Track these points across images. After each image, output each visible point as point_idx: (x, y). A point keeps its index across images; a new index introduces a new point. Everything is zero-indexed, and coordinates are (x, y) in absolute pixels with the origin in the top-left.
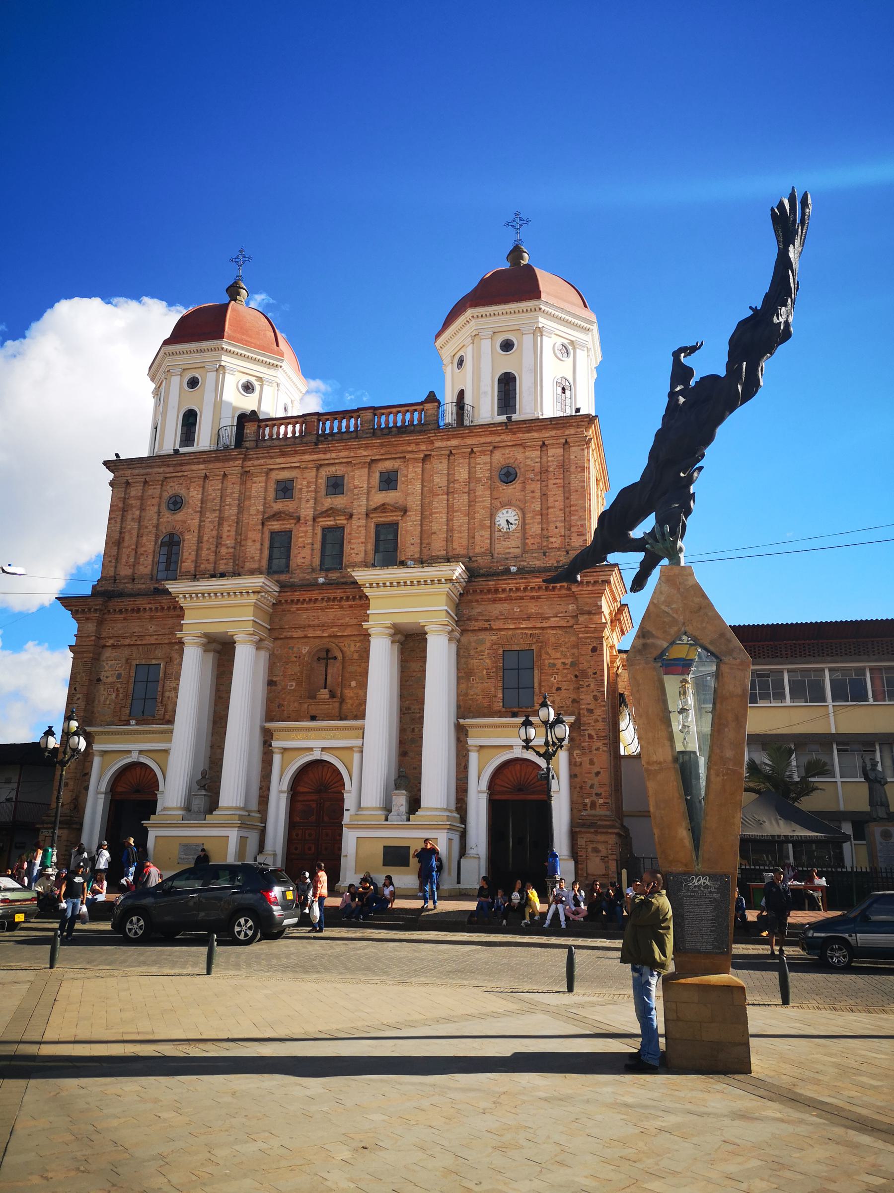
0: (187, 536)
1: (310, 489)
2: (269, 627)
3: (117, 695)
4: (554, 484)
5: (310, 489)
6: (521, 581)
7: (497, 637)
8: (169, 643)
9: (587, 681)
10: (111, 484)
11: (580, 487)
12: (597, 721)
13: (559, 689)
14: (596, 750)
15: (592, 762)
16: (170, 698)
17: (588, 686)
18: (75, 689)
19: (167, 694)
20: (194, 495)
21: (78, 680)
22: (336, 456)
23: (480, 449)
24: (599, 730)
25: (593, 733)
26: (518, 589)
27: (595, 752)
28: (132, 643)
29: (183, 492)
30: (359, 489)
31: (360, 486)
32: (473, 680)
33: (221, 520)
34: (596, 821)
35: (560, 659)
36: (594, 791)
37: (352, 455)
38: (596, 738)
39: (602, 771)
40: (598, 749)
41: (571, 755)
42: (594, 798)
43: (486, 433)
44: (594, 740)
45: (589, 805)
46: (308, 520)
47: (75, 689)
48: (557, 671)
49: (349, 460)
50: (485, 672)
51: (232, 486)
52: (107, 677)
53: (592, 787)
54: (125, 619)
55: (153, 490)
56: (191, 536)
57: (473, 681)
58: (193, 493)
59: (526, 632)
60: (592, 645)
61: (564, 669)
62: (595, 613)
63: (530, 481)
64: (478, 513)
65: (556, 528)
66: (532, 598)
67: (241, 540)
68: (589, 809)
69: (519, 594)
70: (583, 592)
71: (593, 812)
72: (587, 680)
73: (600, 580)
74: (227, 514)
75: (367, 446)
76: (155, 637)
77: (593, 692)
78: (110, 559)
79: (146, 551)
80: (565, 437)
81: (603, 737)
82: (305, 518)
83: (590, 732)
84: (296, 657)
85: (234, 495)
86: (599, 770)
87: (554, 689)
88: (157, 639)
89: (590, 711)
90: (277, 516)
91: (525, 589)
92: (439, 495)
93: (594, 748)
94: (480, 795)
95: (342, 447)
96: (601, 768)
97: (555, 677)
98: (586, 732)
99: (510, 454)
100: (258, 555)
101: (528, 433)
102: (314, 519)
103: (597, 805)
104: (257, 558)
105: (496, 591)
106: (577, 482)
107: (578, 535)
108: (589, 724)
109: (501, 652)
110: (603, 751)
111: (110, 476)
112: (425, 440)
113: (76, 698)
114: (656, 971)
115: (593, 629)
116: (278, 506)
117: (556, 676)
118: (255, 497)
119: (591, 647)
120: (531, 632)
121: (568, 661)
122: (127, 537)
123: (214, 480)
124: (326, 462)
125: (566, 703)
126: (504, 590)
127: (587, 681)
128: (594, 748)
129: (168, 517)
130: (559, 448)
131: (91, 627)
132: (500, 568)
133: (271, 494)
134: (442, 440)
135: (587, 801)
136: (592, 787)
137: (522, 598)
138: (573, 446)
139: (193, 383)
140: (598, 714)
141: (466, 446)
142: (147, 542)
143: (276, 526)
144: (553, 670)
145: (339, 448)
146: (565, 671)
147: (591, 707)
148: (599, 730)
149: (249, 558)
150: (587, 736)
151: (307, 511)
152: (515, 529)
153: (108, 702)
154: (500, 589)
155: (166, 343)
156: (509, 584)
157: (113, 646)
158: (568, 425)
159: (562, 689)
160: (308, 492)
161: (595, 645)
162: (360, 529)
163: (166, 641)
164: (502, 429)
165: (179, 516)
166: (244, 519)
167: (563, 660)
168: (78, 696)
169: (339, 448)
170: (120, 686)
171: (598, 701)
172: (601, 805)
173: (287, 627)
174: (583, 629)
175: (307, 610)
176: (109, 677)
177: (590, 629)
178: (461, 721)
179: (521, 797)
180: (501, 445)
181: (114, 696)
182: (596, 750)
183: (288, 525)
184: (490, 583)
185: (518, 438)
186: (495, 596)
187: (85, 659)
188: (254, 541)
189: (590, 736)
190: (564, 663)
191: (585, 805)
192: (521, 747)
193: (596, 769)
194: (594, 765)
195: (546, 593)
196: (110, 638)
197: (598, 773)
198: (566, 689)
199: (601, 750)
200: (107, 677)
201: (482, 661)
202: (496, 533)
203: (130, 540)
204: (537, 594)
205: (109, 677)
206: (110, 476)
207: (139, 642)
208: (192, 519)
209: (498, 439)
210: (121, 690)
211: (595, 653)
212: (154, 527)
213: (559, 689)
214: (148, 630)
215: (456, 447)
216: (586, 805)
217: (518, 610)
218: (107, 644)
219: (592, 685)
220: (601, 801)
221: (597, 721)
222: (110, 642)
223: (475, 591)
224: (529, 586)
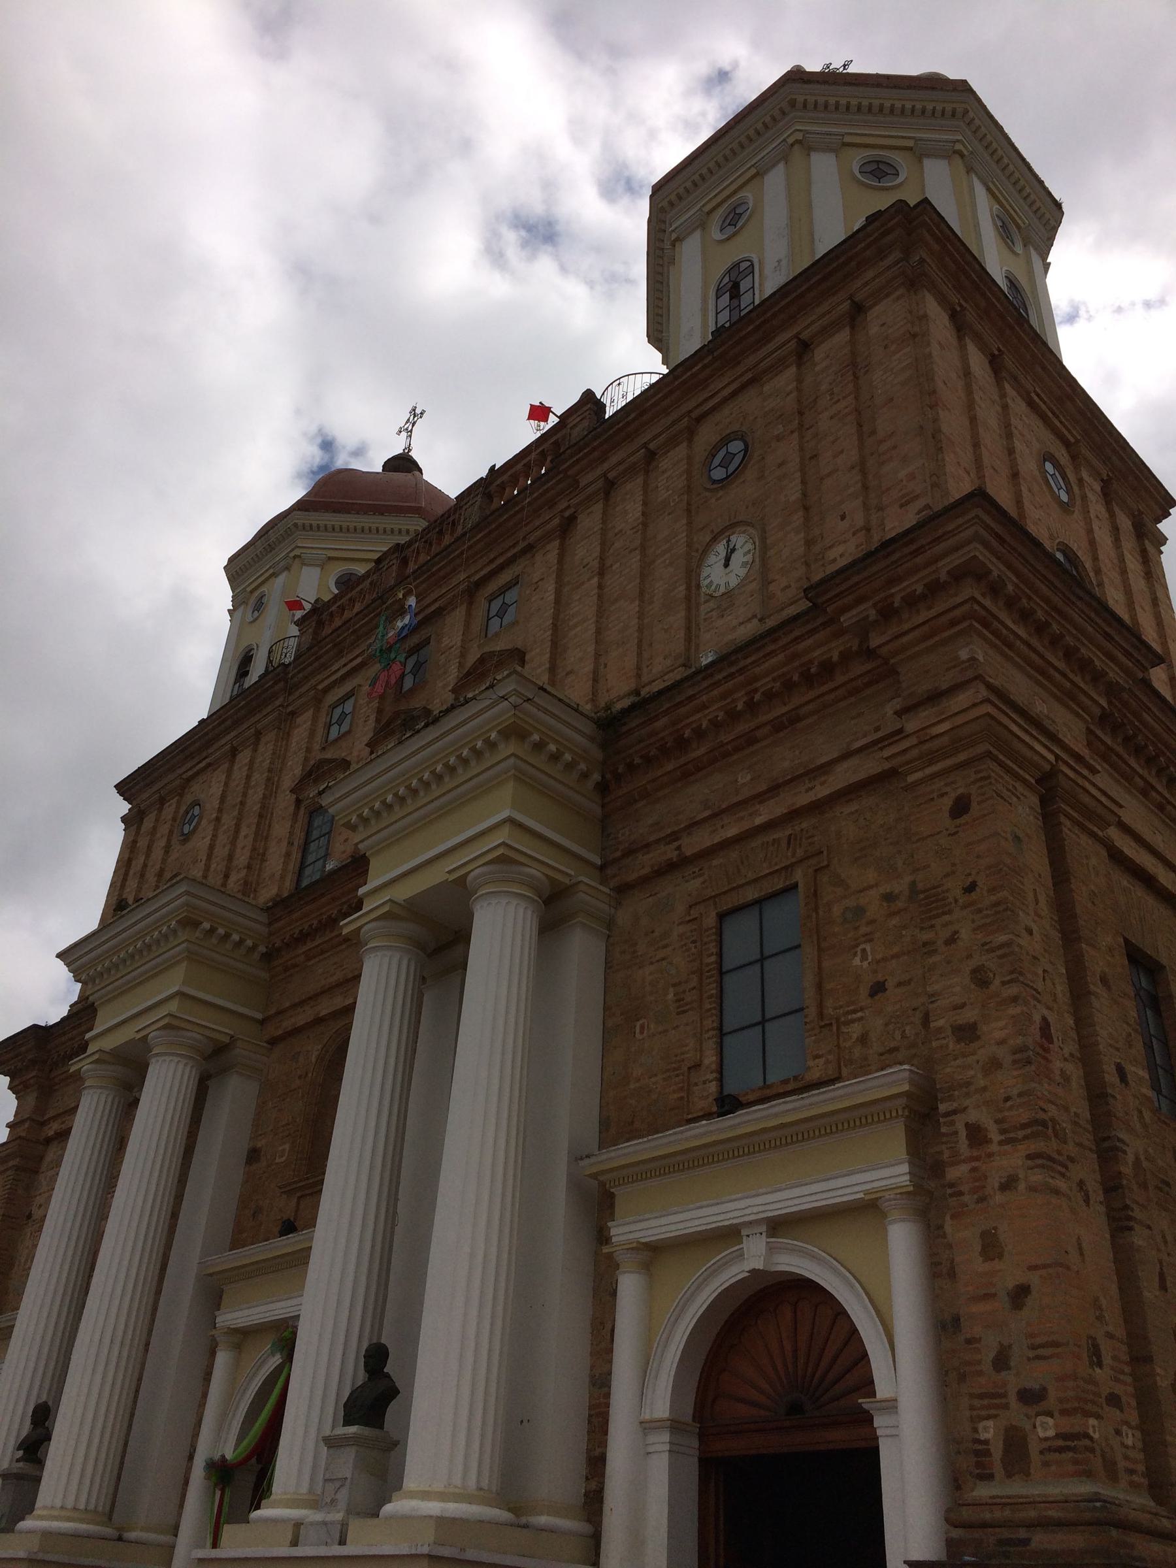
2: (259, 1016)
4: (831, 418)
6: (730, 684)
7: (701, 879)
9: (945, 925)
10: (124, 819)
12: (994, 1065)
13: (878, 989)
15: (991, 1247)
17: (952, 940)
24: (1007, 1099)
26: (733, 716)
27: (999, 1198)
32: (642, 1027)
34: (1022, 1534)
35: (876, 885)
36: (1013, 1382)
39: (1034, 1279)
40: (1008, 1185)
42: (1016, 1413)
44: (994, 1147)
45: (997, 1451)
48: (868, 929)
50: (671, 996)
53: (1001, 1361)
57: (642, 1033)
59: (776, 836)
60: (953, 795)
61: (891, 915)
66: (778, 726)
68: (998, 1469)
69: (742, 727)
70: (905, 639)
71: (1016, 1488)
72: (947, 918)
73: (943, 576)
77: (970, 956)
81: (1024, 1126)
83: (973, 1116)
87: (864, 991)
89: (967, 1033)
91: (752, 706)
92: (583, 583)
93: (994, 1182)
96: (1033, 1268)
97: (864, 950)
103: (1034, 1448)
105: (682, 744)
107: (902, 506)
108: (968, 1084)
109: (711, 920)
110: (1032, 1189)
111: (124, 807)
115: (945, 740)
117: (868, 947)
119: (948, 802)
120: (788, 832)
121: (900, 886)
125: (904, 1036)
126: (700, 734)
127: (945, 925)
128: (994, 1182)
131: (31, 1099)
135: (989, 1431)
136: (1001, 1361)
137: (750, 740)
140: (998, 1035)
144: (856, 928)
146: (895, 921)
147: (969, 1015)
148: (1007, 1099)
150: (963, 1133)
156: (704, 707)
158: (853, 264)
159: (890, 984)
161: (960, 791)
164: (705, 367)
167: (885, 888)
171: (993, 987)
174: (915, 753)
175: (323, 952)
177: (936, 743)
184: (659, 724)
186: (682, 760)
189: (976, 1135)
190: (889, 898)
191: (981, 1452)
192: (764, 1228)
193: (1010, 1274)
194: (1001, 1256)
195: (812, 694)
197: (1020, 1294)
198: (899, 984)
199: (1022, 1186)
201: (664, 963)
204: (785, 709)
206: (124, 807)
211: (965, 818)
213: (878, 989)
216: (988, 1453)
217: (749, 777)
219: (965, 934)
220: (1046, 1428)
221: (994, 1065)
223: (631, 768)
224: (756, 691)
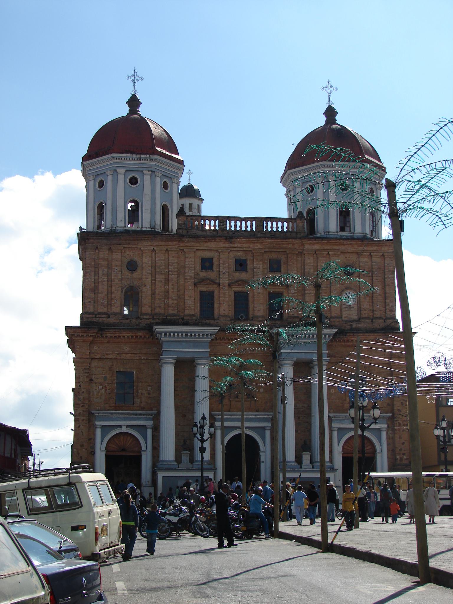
0: (144, 289)
1: (225, 266)
3: (106, 390)
5: (225, 266)
8: (140, 359)
11: (390, 283)
14: (403, 431)
16: (143, 394)
18: (80, 386)
19: (140, 391)
20: (146, 261)
21: (81, 380)
22: (241, 246)
23: (333, 253)
25: (401, 422)
28: (114, 357)
29: (137, 259)
30: (257, 269)
31: (258, 267)
33: (167, 281)
37: (251, 246)
38: (402, 425)
41: (387, 433)
42: (401, 456)
43: (337, 243)
46: (225, 286)
47: (80, 386)
49: (250, 249)
51: (172, 258)
52: (97, 378)
54: (108, 342)
55: (116, 256)
56: (147, 290)
58: (145, 260)
62: (402, 357)
63: (362, 276)
64: (333, 292)
65: (378, 306)
67: (180, 295)
74: (170, 277)
75: (262, 242)
76: (129, 355)
78: (89, 300)
79: (115, 297)
80: (383, 252)
82: (223, 284)
83: (399, 422)
84: (224, 372)
85: (174, 265)
86: (403, 441)
88: (131, 356)
90: (202, 281)
94: (102, 452)
95: (245, 241)
98: (397, 422)
99: (349, 257)
100: (193, 306)
101: (361, 247)
102: (229, 285)
104: (193, 308)
106: (389, 280)
112: (299, 243)
113: (81, 392)
114: (142, 512)
116: (203, 274)
118: (188, 267)
122: (100, 287)
123: (159, 253)
124: (235, 249)
129: (128, 275)
130: (378, 257)
132: (347, 327)
133: (199, 267)
134: (310, 244)
138: (387, 258)
139: (134, 181)
141: (325, 250)
142: (115, 290)
143: (204, 288)
145: (244, 241)
147: (400, 408)
149: (187, 307)
151: (224, 280)
152: (354, 304)
153: (100, 394)
154: (350, 341)
155: (85, 158)
157: (100, 359)
160: (224, 268)
162: (259, 295)
163: (138, 358)
165: (136, 274)
166: (181, 281)
168: (83, 390)
169: (244, 241)
170: (107, 385)
172: (405, 459)
173: (219, 354)
176: (98, 378)
178: (329, 414)
179: (124, 453)
180: (345, 251)
181: (103, 391)
182: (403, 431)
183: (211, 288)
185: (355, 249)
187: (85, 367)
188: (190, 297)
189: (400, 424)
196: (98, 353)
197: (403, 443)
200: (97, 378)
202: (343, 305)
203: (103, 288)
205: (98, 378)
207: (119, 358)
208: (147, 278)
209: (343, 248)
210: (108, 388)
212: (119, 281)
214: (124, 350)
215: (318, 250)
218: (96, 358)
220: (405, 457)
222: (98, 356)
